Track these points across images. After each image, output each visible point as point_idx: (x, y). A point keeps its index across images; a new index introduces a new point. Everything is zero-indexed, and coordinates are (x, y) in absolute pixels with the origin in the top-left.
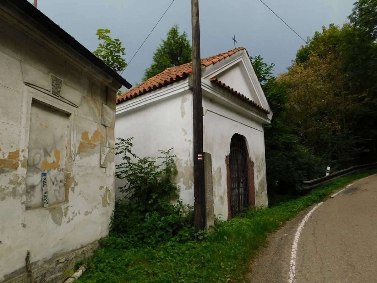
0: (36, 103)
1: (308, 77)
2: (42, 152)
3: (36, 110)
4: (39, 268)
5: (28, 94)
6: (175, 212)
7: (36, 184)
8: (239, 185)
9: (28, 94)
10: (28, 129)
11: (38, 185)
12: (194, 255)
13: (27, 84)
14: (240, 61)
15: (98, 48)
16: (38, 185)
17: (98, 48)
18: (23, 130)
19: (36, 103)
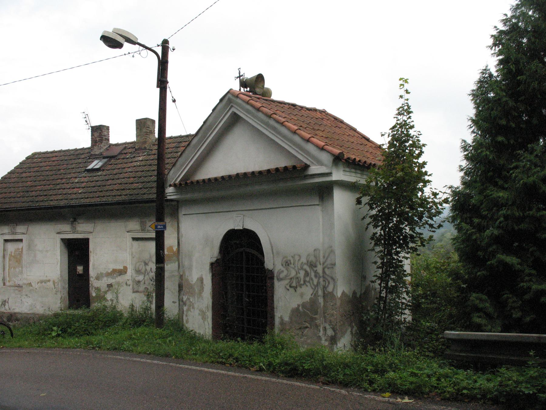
0: (134, 239)
1: (462, 300)
2: (143, 264)
3: (136, 243)
4: (382, 305)
5: (129, 236)
6: (417, 156)
7: (141, 280)
8: (324, 272)
9: (129, 236)
10: (130, 253)
11: (142, 281)
12: (393, 141)
13: (128, 232)
14: (233, 336)
15: (388, 137)
16: (142, 281)
17: (388, 137)
18: (128, 255)
19: (134, 239)
